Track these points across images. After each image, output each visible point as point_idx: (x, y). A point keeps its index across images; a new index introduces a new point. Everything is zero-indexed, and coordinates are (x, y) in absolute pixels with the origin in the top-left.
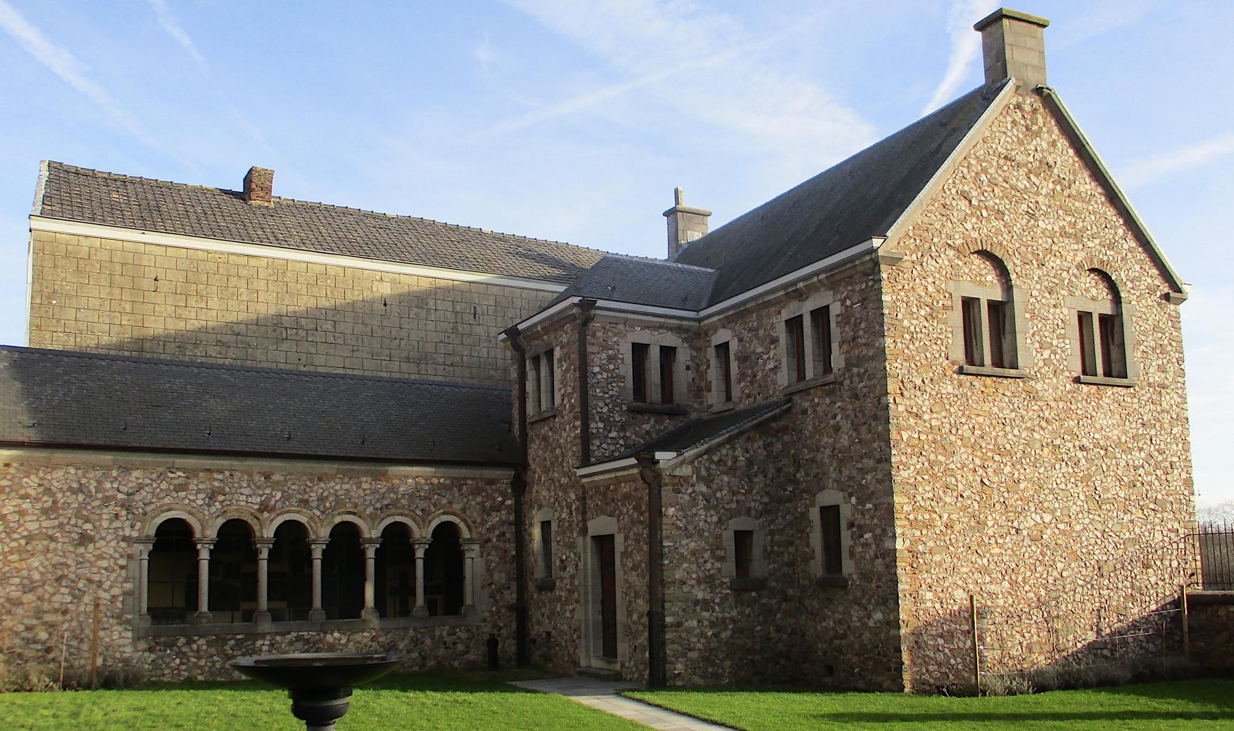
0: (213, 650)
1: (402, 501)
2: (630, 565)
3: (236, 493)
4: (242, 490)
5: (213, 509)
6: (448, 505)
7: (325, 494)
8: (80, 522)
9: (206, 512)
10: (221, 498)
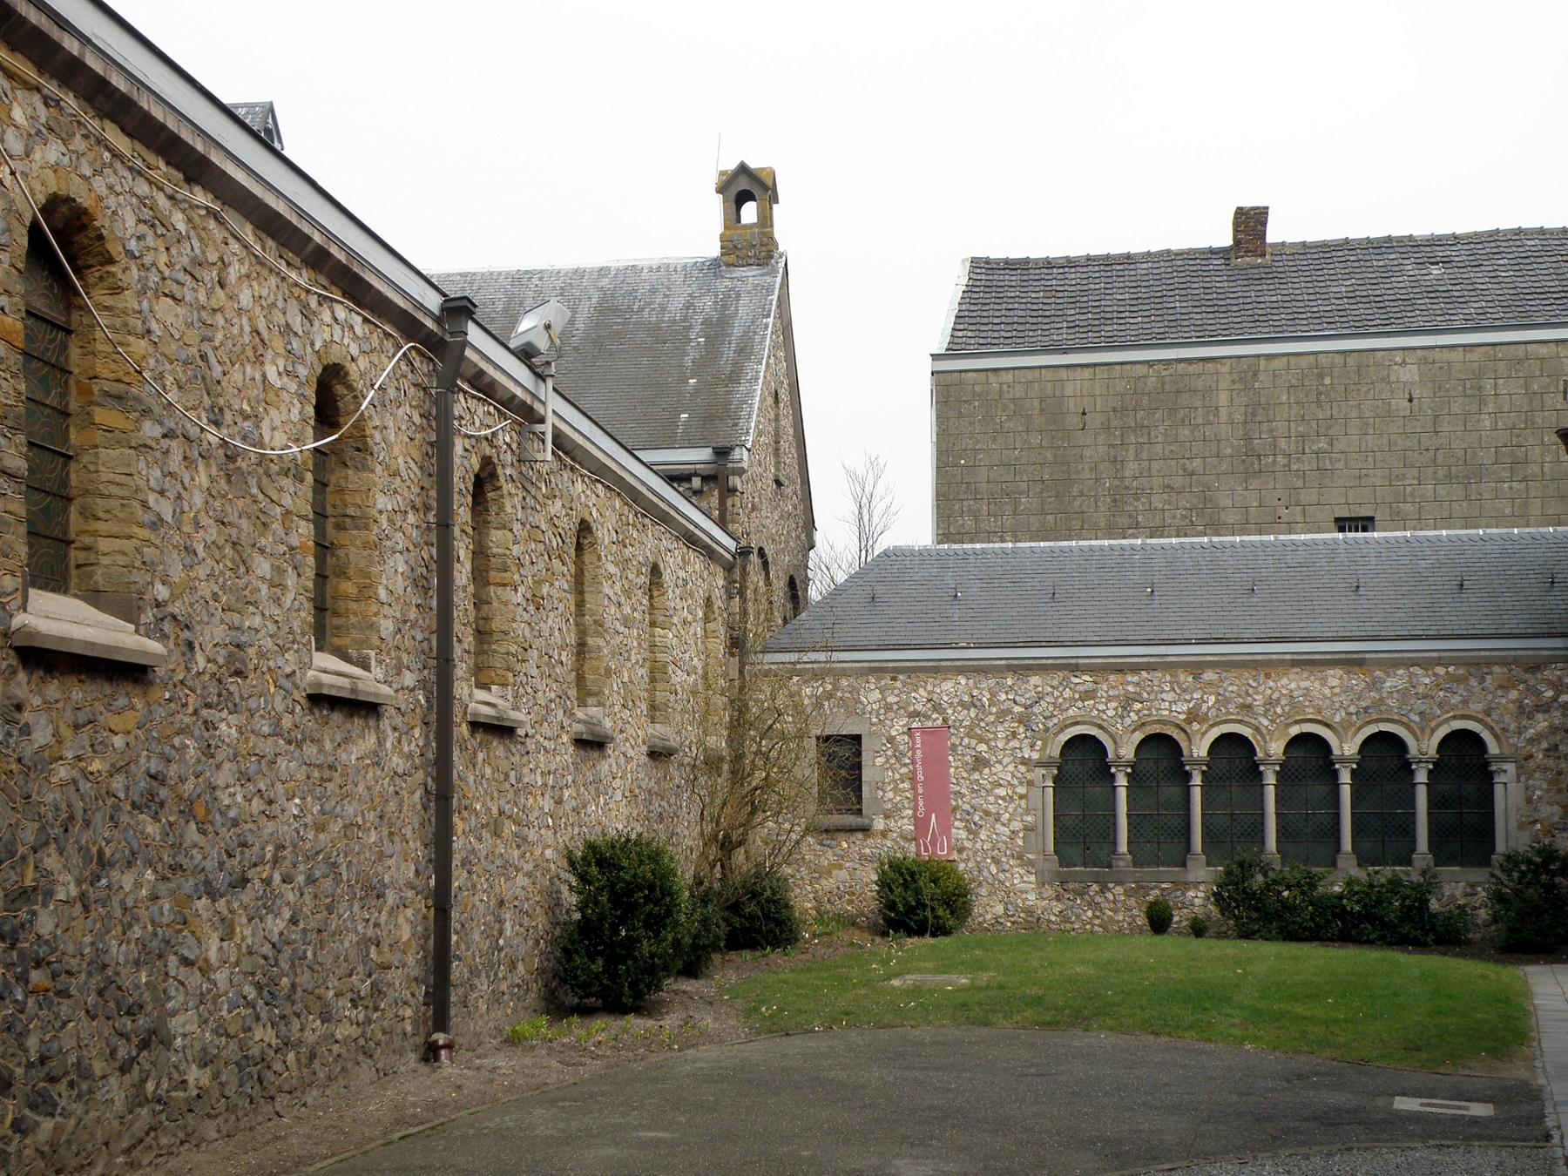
0: (1132, 902)
1: (1390, 702)
3: (1156, 699)
4: (1164, 696)
5: (1128, 721)
7: (1275, 696)
8: (974, 742)
10: (1138, 706)
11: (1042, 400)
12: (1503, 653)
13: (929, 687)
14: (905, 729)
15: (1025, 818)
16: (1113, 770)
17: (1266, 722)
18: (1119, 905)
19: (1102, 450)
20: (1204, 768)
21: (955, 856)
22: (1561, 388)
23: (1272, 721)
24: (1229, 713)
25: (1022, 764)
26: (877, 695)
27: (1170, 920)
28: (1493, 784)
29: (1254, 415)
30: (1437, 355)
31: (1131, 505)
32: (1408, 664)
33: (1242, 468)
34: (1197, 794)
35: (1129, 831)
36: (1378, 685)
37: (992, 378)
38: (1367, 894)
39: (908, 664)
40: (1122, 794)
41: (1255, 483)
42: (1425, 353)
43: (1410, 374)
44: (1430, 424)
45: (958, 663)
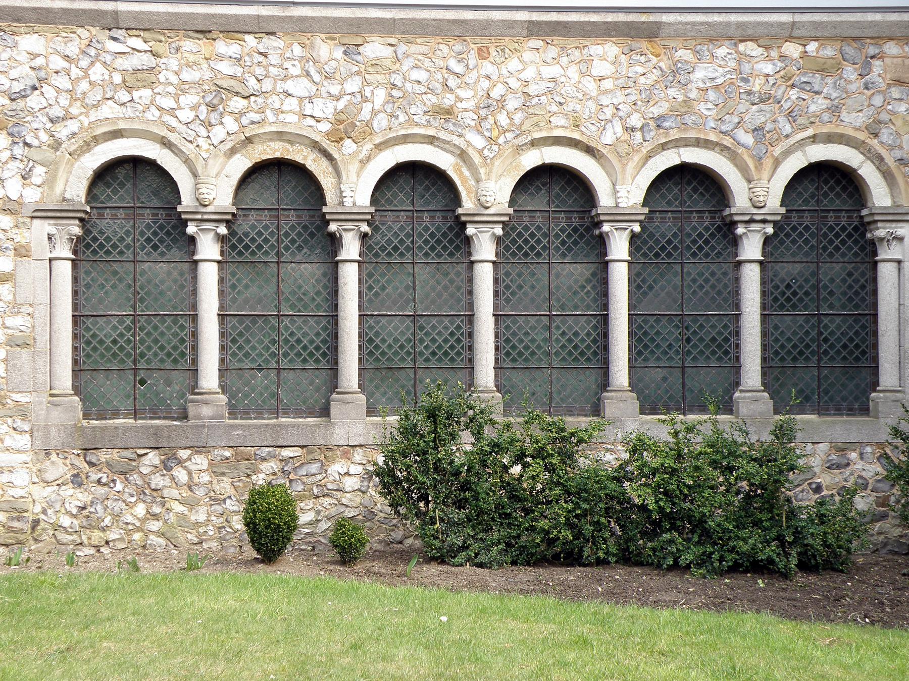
0: (225, 486)
1: (702, 107)
2: (575, 441)
4: (290, 86)
5: (218, 133)
6: (826, 116)
7: (496, 93)
9: (201, 141)
10: (238, 103)
15: (10, 321)
16: (191, 229)
17: (478, 142)
18: (200, 492)
20: (365, 228)
24: (412, 123)
27: (291, 525)
28: (876, 263)
35: (222, 348)
38: (673, 472)
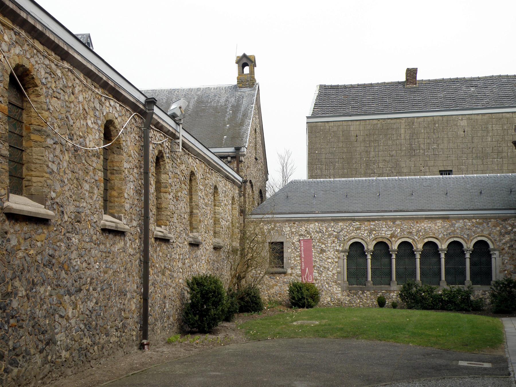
0: (373, 297)
1: (457, 231)
3: (380, 230)
4: (383, 229)
5: (371, 237)
7: (419, 229)
8: (320, 244)
10: (374, 232)
11: (343, 132)
12: (495, 215)
13: (306, 226)
14: (298, 240)
15: (337, 269)
16: (366, 253)
17: (416, 238)
18: (368, 298)
19: (363, 148)
20: (396, 253)
21: (314, 282)
22: (514, 128)
23: (419, 237)
24: (404, 235)
25: (336, 251)
26: (288, 229)
28: (491, 258)
29: (413, 137)
30: (473, 117)
31: (372, 166)
32: (463, 218)
33: (409, 154)
34: (394, 261)
35: (371, 274)
36: (454, 226)
37: (326, 124)
38: (450, 294)
39: (299, 219)
40: (369, 261)
41: (413, 159)
42: (469, 116)
43: (464, 123)
44: (471, 139)
45: (315, 218)
